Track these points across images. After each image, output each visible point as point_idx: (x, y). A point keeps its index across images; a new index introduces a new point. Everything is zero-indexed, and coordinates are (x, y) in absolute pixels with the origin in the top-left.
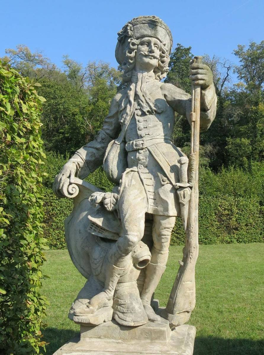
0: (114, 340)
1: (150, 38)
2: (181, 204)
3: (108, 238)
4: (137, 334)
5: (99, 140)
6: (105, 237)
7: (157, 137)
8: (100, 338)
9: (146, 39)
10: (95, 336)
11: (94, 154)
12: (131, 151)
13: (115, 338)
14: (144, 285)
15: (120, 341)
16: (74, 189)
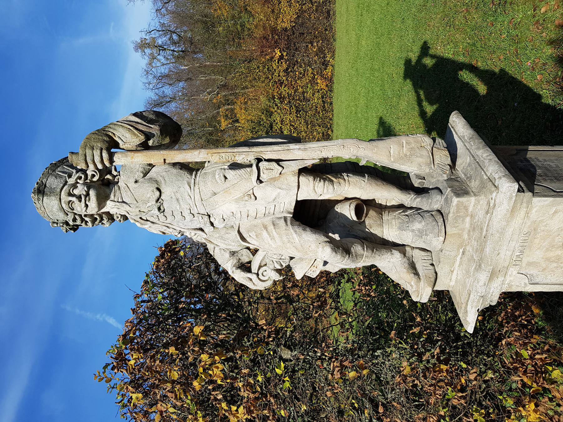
4: (455, 232)
7: (193, 198)
13: (456, 256)
15: (461, 251)
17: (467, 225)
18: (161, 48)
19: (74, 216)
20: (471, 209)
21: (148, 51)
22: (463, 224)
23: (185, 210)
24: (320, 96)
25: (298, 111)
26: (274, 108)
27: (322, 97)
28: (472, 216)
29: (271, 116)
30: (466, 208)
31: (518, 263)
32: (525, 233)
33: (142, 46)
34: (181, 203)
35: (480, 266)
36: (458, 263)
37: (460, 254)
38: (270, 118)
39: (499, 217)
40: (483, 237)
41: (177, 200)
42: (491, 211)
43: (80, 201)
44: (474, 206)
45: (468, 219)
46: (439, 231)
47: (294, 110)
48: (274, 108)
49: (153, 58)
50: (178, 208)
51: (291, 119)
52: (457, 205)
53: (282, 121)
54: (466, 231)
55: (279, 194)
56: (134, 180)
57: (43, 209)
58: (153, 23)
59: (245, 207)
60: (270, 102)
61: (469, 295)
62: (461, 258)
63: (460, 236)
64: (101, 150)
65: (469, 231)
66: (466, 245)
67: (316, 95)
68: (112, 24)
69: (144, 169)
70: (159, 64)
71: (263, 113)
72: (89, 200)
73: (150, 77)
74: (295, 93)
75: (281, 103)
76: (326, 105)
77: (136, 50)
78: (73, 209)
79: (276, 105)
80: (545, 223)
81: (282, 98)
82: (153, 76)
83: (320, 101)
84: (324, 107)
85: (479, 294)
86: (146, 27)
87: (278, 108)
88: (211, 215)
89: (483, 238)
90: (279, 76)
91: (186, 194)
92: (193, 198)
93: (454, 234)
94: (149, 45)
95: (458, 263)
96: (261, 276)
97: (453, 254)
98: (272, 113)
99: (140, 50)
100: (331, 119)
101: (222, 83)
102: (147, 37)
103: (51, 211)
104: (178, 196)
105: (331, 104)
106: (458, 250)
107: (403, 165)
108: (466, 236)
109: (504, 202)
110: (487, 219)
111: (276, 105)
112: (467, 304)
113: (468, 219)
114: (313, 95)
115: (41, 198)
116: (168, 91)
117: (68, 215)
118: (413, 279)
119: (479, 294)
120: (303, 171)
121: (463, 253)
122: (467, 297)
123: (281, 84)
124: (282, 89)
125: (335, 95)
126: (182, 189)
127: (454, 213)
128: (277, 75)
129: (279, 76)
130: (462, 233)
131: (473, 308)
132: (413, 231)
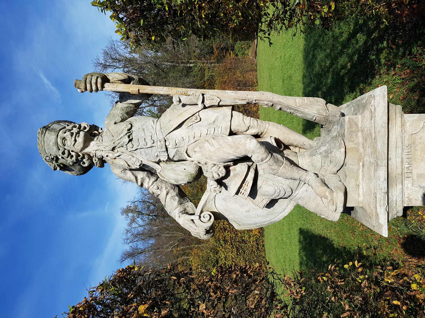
0: (361, 170)
1: (59, 137)
2: (220, 104)
3: (253, 176)
4: (353, 146)
5: (158, 192)
6: (252, 180)
7: (154, 128)
8: (358, 186)
9: (59, 140)
10: (357, 191)
11: (172, 197)
12: (167, 152)
13: (358, 169)
14: (300, 146)
15: (361, 164)
16: (205, 216)
17: (361, 140)
18: (140, 213)
19: (64, 151)
20: (360, 125)
21: (130, 215)
22: (357, 138)
23: (148, 137)
24: (255, 240)
25: (238, 250)
26: (220, 248)
27: (256, 240)
28: (362, 130)
29: (217, 253)
30: (356, 124)
31: (410, 175)
32: (407, 145)
33: (127, 211)
34: (146, 132)
35: (377, 164)
36: (361, 177)
37: (361, 168)
38: (217, 255)
39: (381, 114)
40: (373, 139)
41: (143, 129)
42: (373, 116)
43: (72, 136)
44: (362, 122)
45: (360, 134)
46: (340, 145)
47: (235, 250)
48: (220, 248)
49: (133, 220)
50: (143, 135)
51: (233, 256)
52: (349, 121)
53: (226, 258)
54: (361, 145)
55: (217, 117)
56: (114, 122)
57: (42, 143)
58: (137, 197)
59: (192, 131)
60: (217, 243)
61: (376, 197)
62: (363, 171)
63: (357, 150)
64: (97, 78)
65: (363, 144)
66: (364, 158)
67: (252, 238)
68: (108, 203)
69: (123, 115)
70: (136, 226)
71: (211, 251)
72: (79, 136)
73: (129, 234)
74: (235, 237)
75: (225, 243)
76: (259, 246)
77: (122, 214)
78: (64, 145)
79: (221, 245)
80: (420, 136)
81: (225, 241)
82: (131, 233)
83: (255, 243)
84: (258, 248)
85: (383, 191)
86: (132, 199)
87: (222, 248)
88: (167, 140)
89: (373, 140)
90: (224, 224)
91: (150, 126)
92: (154, 128)
93: (352, 148)
94: (132, 211)
95: (361, 177)
96: (202, 219)
97: (355, 167)
98: (218, 251)
99: (125, 214)
100: (264, 258)
101: (181, 238)
102: (132, 206)
103: (48, 145)
104: (144, 127)
105: (263, 246)
106: (359, 164)
107: (306, 108)
108: (362, 150)
109: (381, 101)
110: (373, 122)
111: (221, 245)
112: (376, 208)
113: (360, 134)
114: (249, 239)
115: (45, 131)
116: (141, 245)
117: (59, 150)
118: (327, 190)
119: (383, 191)
120: (234, 108)
121: (363, 166)
122: (375, 201)
123: (225, 230)
124: (226, 234)
125: (265, 239)
126: (148, 123)
127: (348, 128)
128: (222, 224)
129: (224, 224)
130: (358, 147)
131: (382, 207)
132: (321, 154)
